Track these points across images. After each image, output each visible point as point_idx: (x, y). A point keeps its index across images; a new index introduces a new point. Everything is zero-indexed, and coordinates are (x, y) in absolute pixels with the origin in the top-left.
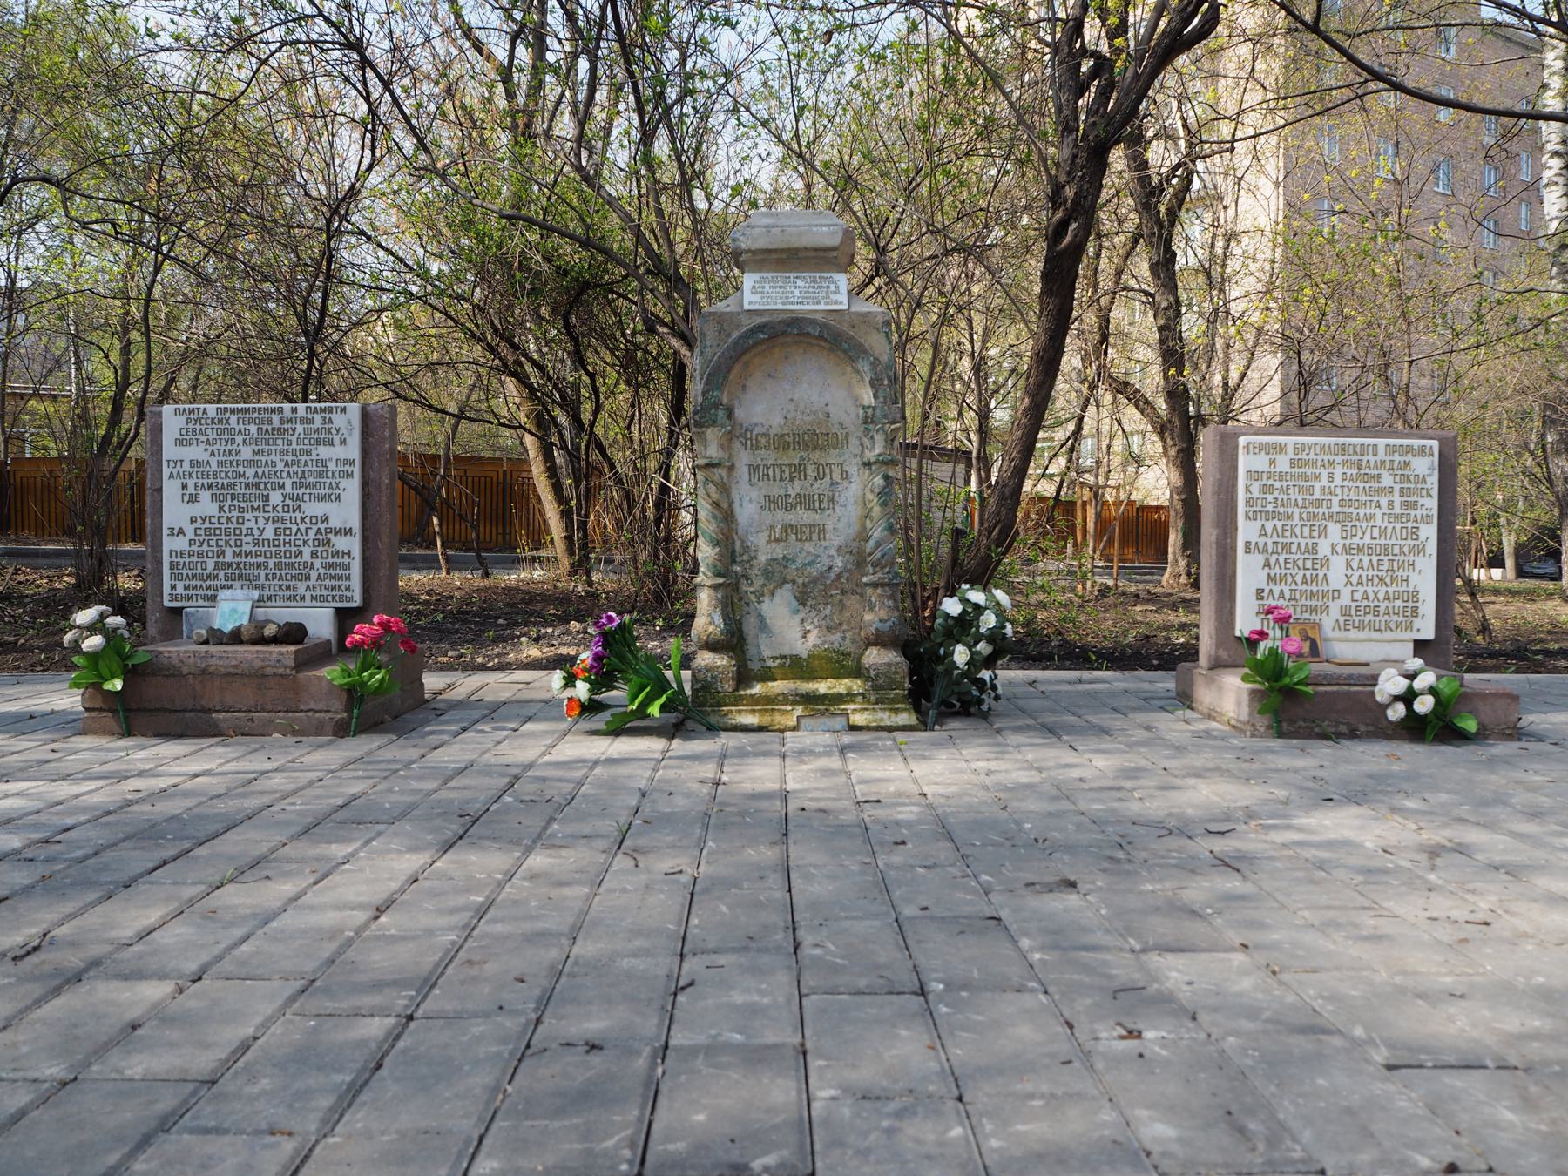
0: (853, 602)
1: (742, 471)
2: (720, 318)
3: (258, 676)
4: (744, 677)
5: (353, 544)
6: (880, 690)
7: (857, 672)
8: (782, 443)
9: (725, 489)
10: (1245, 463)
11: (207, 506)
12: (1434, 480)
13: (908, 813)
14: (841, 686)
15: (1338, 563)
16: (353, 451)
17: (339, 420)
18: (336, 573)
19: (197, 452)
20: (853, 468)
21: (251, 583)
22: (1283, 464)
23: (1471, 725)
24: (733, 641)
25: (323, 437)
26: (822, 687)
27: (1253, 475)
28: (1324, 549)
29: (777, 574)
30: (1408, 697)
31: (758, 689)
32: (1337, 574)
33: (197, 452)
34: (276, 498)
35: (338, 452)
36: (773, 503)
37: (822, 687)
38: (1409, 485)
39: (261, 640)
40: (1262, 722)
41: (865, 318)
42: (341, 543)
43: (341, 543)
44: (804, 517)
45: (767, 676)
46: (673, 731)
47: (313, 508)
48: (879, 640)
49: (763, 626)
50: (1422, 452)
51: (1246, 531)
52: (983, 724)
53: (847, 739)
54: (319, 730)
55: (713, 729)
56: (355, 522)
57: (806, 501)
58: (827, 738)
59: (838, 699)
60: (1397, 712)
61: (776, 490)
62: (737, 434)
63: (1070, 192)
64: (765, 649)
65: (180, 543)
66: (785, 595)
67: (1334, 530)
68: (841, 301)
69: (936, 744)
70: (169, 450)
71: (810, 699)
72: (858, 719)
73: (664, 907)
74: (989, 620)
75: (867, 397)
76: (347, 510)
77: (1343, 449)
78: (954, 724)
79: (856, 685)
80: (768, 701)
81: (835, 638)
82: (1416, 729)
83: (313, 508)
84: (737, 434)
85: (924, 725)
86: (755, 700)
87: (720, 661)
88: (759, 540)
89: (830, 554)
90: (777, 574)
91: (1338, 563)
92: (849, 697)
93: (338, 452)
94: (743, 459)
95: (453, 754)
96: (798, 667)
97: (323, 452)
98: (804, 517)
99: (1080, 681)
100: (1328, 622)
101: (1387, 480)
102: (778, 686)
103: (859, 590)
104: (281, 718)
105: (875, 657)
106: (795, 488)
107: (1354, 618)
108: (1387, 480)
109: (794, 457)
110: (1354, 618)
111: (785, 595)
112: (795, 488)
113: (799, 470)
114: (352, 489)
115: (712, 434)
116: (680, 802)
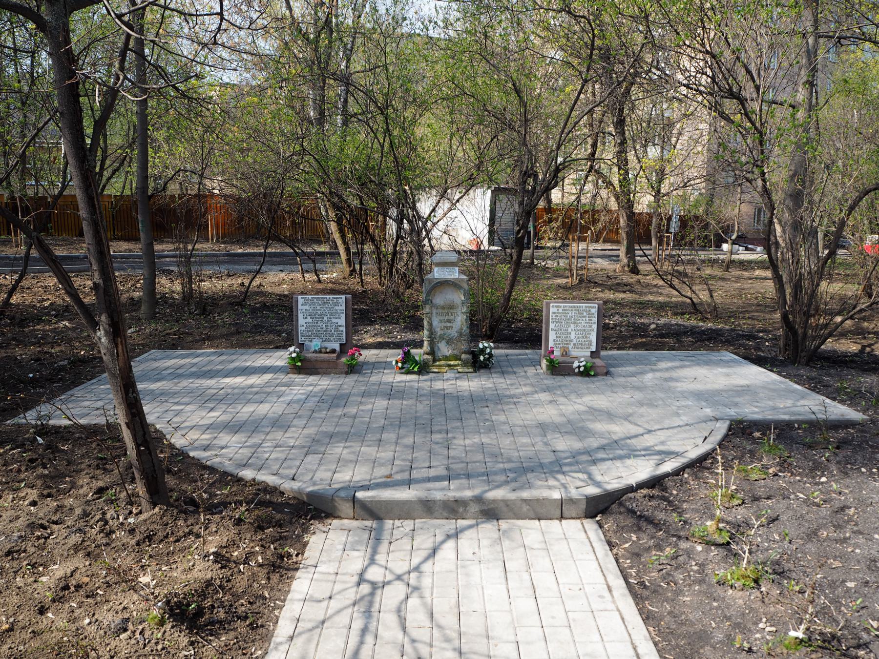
0: (459, 343)
1: (434, 314)
2: (429, 280)
3: (328, 361)
4: (435, 361)
5: (344, 329)
6: (465, 364)
7: (460, 359)
8: (443, 308)
9: (430, 319)
10: (552, 310)
11: (309, 320)
12: (596, 315)
13: (466, 394)
14: (456, 362)
15: (573, 333)
16: (343, 308)
17: (340, 300)
18: (339, 336)
19: (307, 307)
20: (459, 313)
21: (320, 337)
22: (561, 310)
23: (592, 373)
24: (432, 353)
25: (337, 304)
26: (452, 363)
27: (553, 313)
28: (570, 330)
29: (442, 338)
30: (579, 367)
31: (438, 363)
32: (573, 336)
33: (307, 307)
34: (325, 318)
35: (340, 308)
36: (441, 321)
37: (452, 363)
38: (591, 316)
39: (327, 353)
40: (549, 372)
41: (462, 280)
42: (341, 329)
43: (341, 329)
44: (448, 324)
45: (440, 360)
46: (419, 373)
47: (334, 321)
48: (465, 353)
49: (439, 349)
50: (593, 307)
51: (552, 326)
52: (488, 371)
53: (457, 375)
54: (342, 373)
55: (428, 373)
56: (344, 324)
57: (448, 321)
58: (453, 375)
59: (456, 366)
60: (577, 370)
61: (442, 318)
62: (434, 306)
63: (521, 222)
64: (439, 354)
65: (303, 328)
66: (444, 342)
67: (572, 326)
68: (456, 275)
69: (476, 377)
70: (300, 307)
71: (449, 366)
72: (460, 370)
73: (427, 409)
74: (488, 350)
75: (463, 298)
76: (342, 321)
77: (575, 307)
78: (482, 371)
79: (460, 362)
80: (440, 366)
81: (455, 352)
82: (586, 373)
83: (334, 321)
84: (434, 306)
85: (475, 372)
86: (437, 366)
87: (429, 357)
88: (438, 330)
89: (454, 333)
90: (442, 338)
91: (573, 333)
92: (458, 365)
93: (340, 308)
94: (434, 311)
95: (374, 378)
96: (446, 358)
97: (337, 308)
98: (448, 324)
99: (520, 355)
100: (570, 347)
101: (585, 314)
102: (442, 363)
103: (460, 341)
104: (334, 371)
105: (463, 356)
106: (446, 318)
107: (576, 346)
108: (585, 314)
109: (446, 311)
110: (576, 346)
111: (444, 342)
112: (446, 318)
113: (447, 314)
114: (343, 316)
115: (427, 306)
116: (425, 392)
